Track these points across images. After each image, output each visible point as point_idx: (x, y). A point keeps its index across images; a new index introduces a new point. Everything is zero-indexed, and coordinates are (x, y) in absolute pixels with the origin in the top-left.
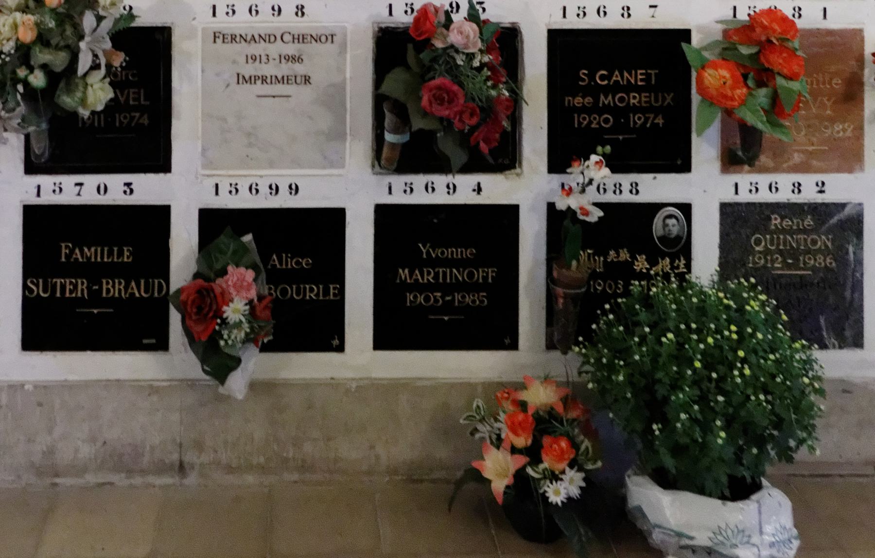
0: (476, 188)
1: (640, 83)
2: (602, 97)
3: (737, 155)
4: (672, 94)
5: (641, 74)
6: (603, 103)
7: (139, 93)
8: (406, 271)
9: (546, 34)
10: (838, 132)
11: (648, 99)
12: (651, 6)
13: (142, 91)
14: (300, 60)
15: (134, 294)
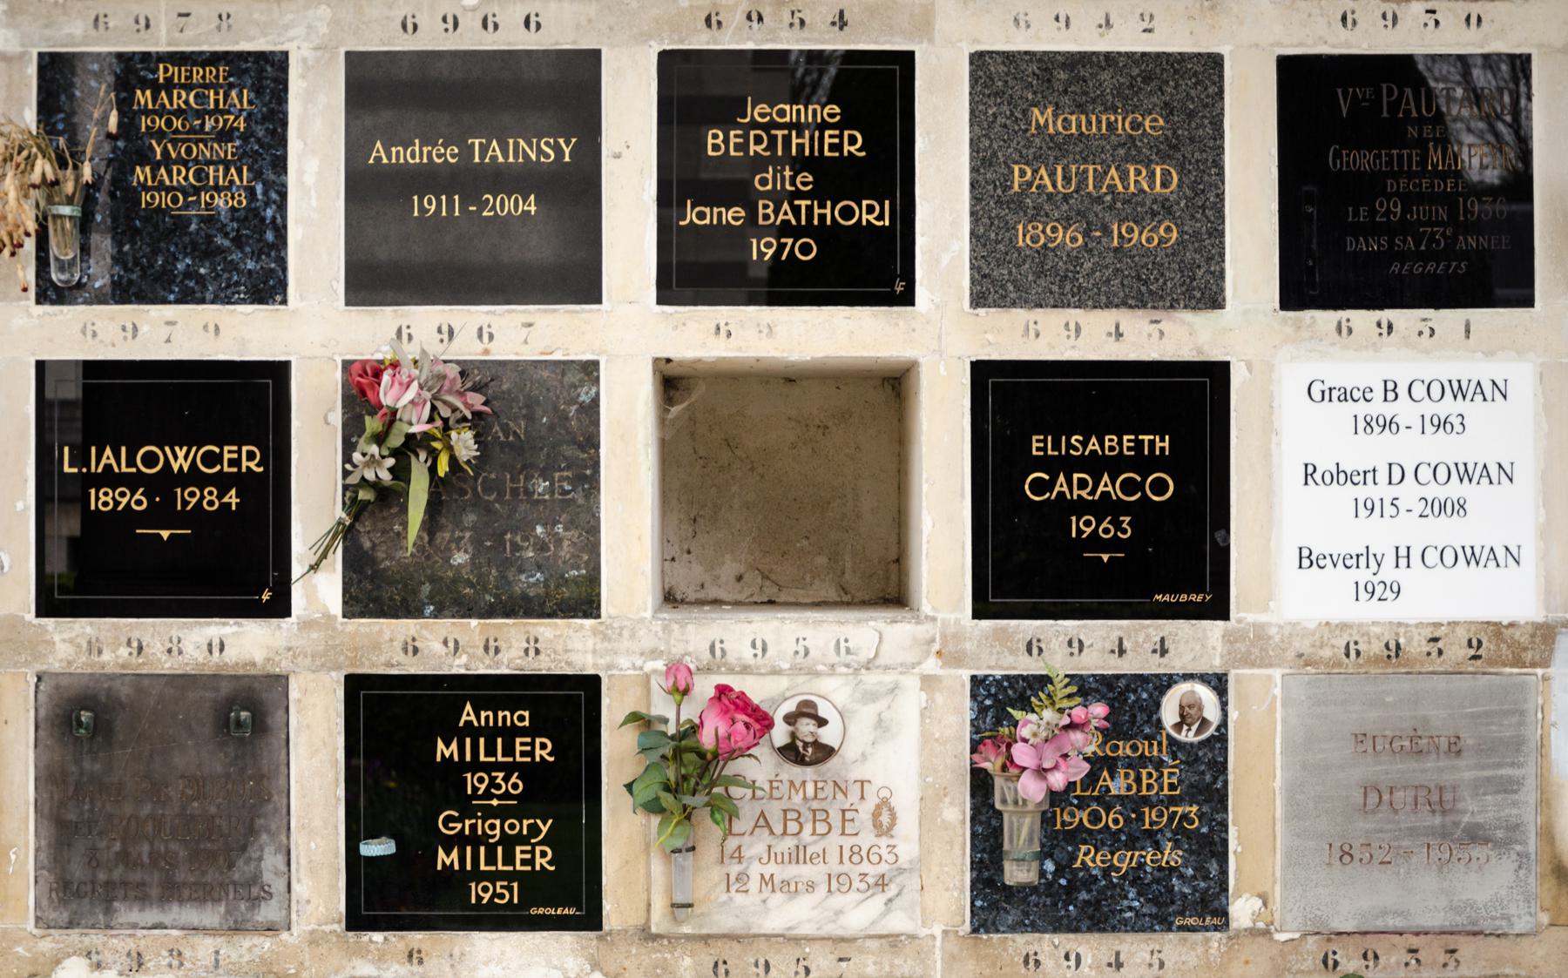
0: (837, 19)
1: (827, 153)
2: (441, 853)
3: (93, 216)
4: (550, 821)
5: (1129, 441)
6: (443, 861)
7: (1045, 441)
8: (148, 93)
9: (1216, 355)
10: (1168, 229)
11: (529, 748)
12: (180, 15)
13: (1050, 438)
14: (1394, 427)
15: (496, 157)
